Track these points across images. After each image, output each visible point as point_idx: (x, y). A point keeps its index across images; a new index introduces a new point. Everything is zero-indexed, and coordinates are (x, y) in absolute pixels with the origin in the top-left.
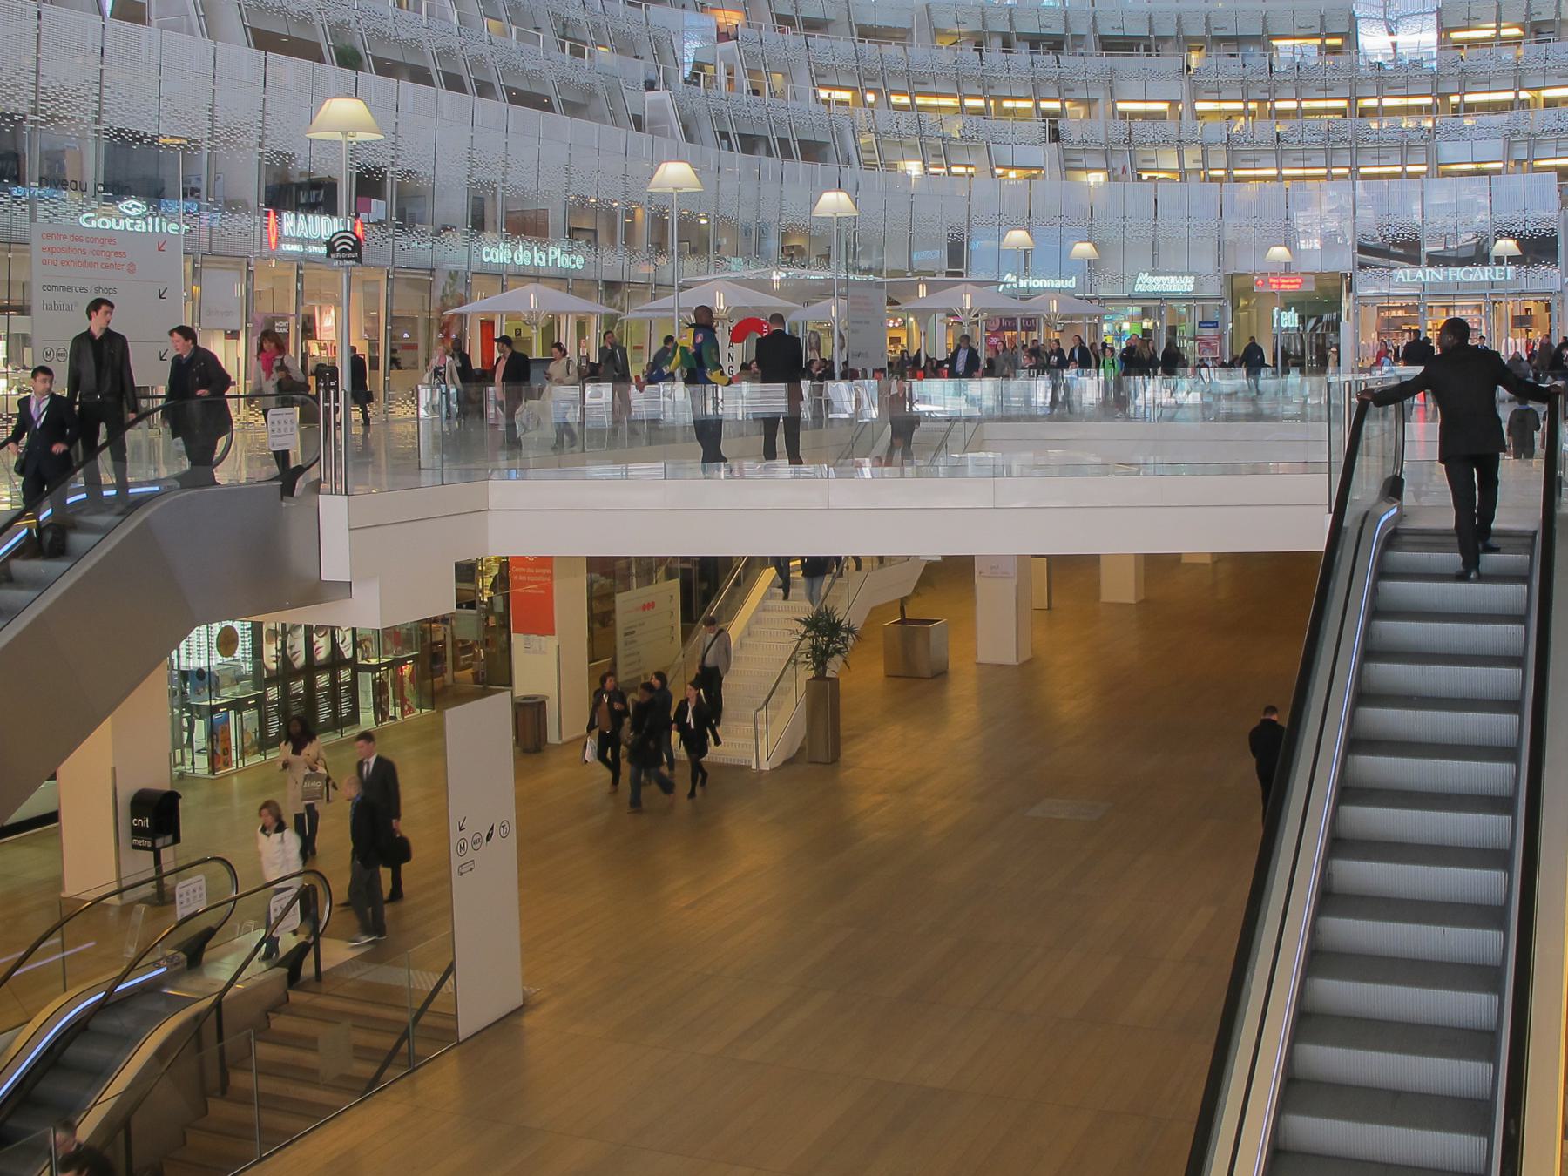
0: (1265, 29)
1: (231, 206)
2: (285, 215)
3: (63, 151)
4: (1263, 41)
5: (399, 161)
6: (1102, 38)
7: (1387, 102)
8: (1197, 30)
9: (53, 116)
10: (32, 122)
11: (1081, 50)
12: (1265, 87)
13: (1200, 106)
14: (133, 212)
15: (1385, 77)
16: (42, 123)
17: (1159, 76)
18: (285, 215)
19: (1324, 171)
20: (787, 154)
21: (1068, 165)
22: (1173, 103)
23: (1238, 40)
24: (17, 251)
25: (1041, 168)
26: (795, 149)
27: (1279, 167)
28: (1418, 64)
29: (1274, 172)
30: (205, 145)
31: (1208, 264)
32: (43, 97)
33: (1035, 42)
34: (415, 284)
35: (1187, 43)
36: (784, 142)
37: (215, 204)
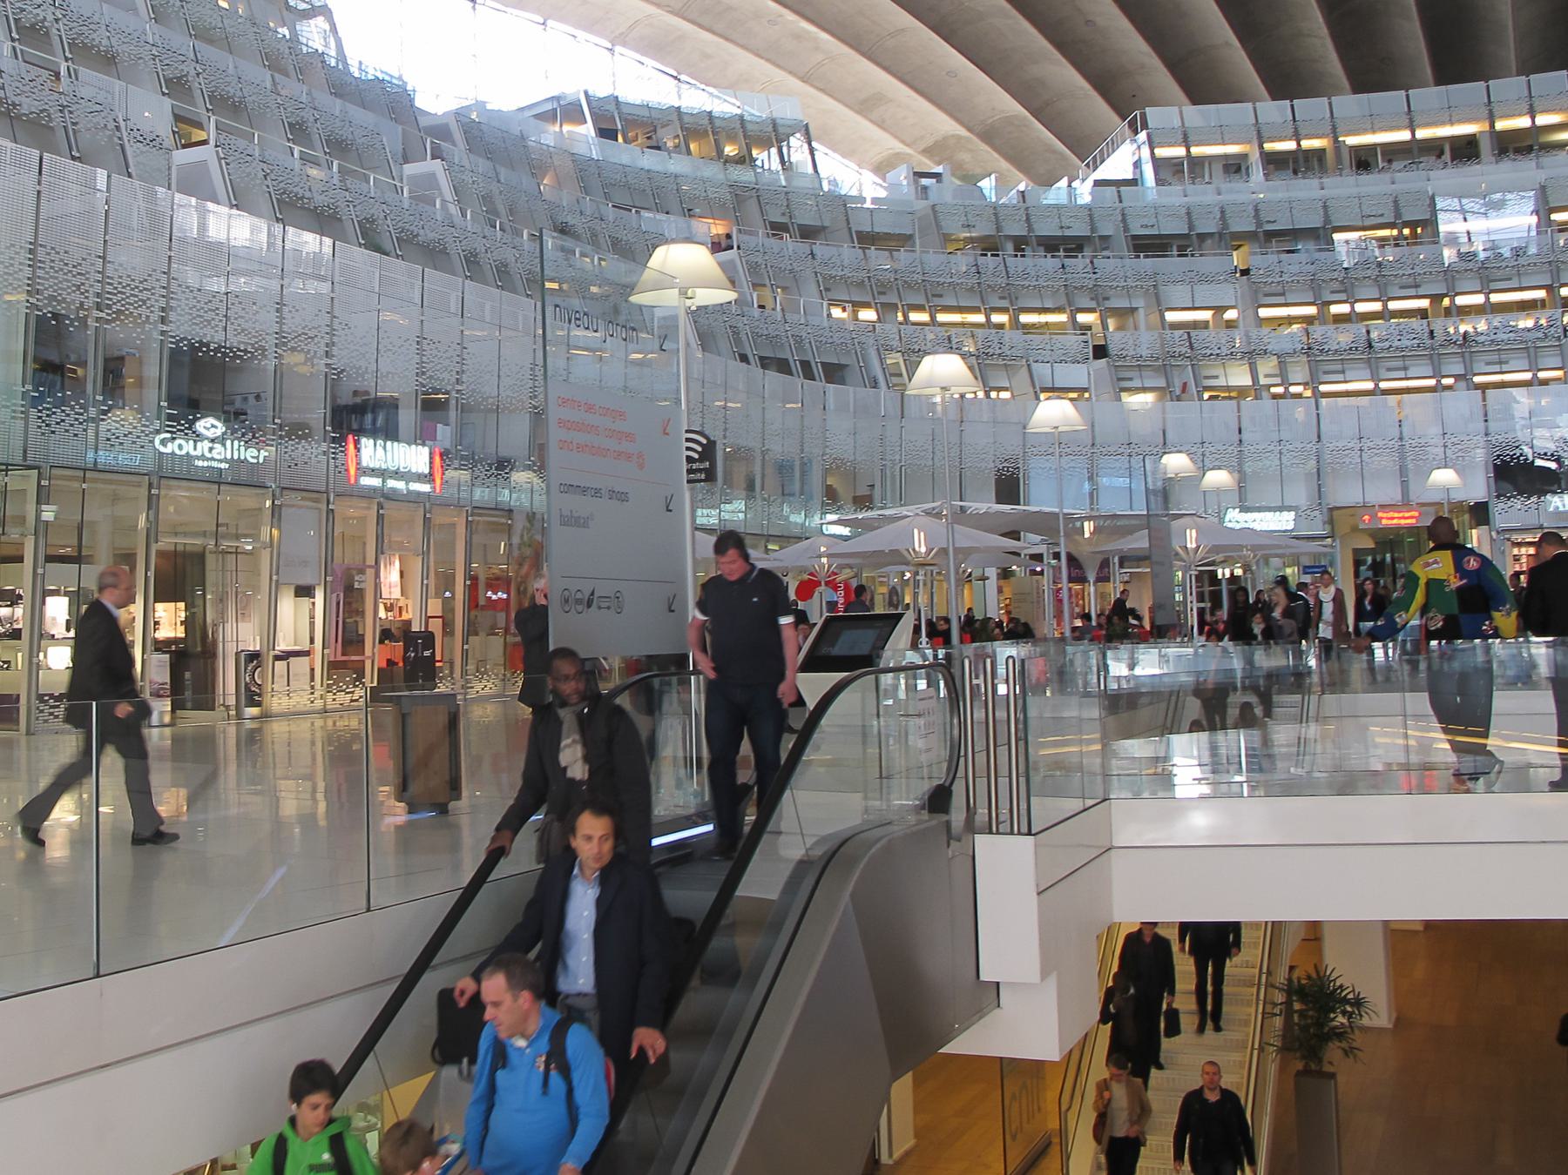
0: (1327, 219)
1: (298, 431)
2: (364, 440)
3: (122, 358)
4: (1321, 235)
5: (465, 377)
6: (1135, 237)
7: (1495, 298)
8: (1244, 225)
9: (119, 312)
10: (98, 319)
11: (1105, 253)
12: (1336, 285)
13: (1264, 312)
14: (210, 434)
15: (1487, 270)
16: (108, 322)
17: (1206, 279)
18: (364, 440)
19: (1432, 382)
20: (808, 374)
21: (1121, 386)
22: (1219, 310)
23: (1295, 234)
24: (95, 480)
25: (1086, 390)
26: (818, 371)
27: (1376, 379)
28: (1518, 252)
29: (1370, 385)
30: (271, 354)
31: (1300, 494)
32: (109, 288)
33: (1051, 245)
34: (496, 528)
35: (1232, 240)
36: (806, 365)
37: (281, 427)
